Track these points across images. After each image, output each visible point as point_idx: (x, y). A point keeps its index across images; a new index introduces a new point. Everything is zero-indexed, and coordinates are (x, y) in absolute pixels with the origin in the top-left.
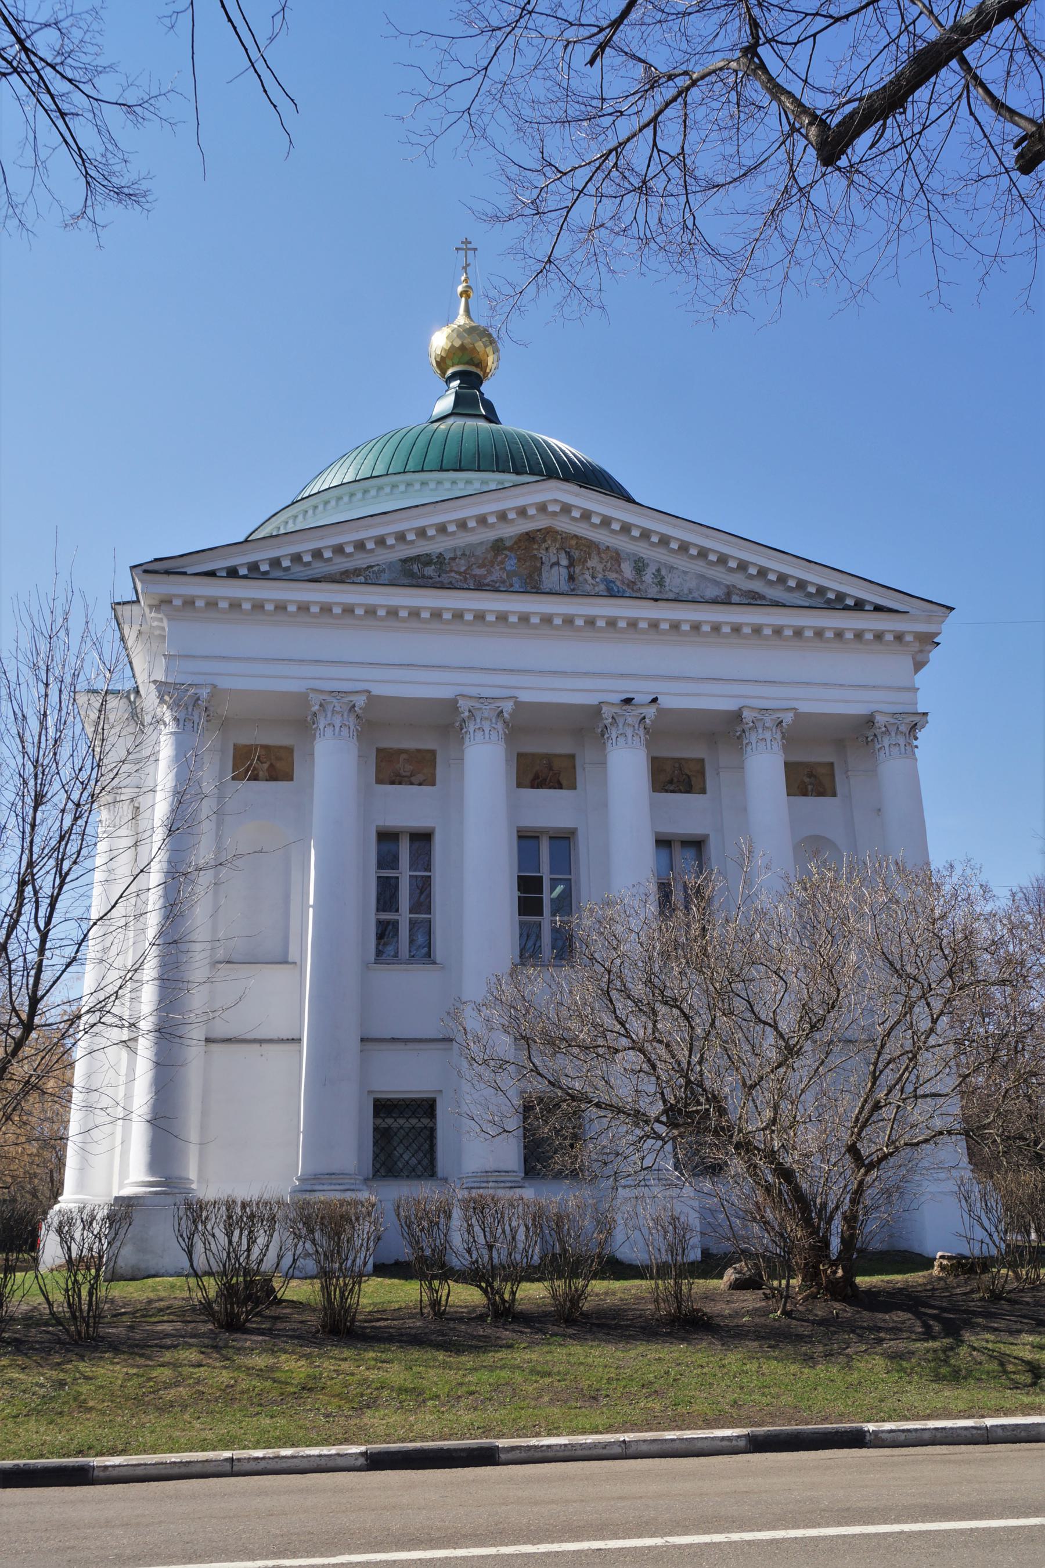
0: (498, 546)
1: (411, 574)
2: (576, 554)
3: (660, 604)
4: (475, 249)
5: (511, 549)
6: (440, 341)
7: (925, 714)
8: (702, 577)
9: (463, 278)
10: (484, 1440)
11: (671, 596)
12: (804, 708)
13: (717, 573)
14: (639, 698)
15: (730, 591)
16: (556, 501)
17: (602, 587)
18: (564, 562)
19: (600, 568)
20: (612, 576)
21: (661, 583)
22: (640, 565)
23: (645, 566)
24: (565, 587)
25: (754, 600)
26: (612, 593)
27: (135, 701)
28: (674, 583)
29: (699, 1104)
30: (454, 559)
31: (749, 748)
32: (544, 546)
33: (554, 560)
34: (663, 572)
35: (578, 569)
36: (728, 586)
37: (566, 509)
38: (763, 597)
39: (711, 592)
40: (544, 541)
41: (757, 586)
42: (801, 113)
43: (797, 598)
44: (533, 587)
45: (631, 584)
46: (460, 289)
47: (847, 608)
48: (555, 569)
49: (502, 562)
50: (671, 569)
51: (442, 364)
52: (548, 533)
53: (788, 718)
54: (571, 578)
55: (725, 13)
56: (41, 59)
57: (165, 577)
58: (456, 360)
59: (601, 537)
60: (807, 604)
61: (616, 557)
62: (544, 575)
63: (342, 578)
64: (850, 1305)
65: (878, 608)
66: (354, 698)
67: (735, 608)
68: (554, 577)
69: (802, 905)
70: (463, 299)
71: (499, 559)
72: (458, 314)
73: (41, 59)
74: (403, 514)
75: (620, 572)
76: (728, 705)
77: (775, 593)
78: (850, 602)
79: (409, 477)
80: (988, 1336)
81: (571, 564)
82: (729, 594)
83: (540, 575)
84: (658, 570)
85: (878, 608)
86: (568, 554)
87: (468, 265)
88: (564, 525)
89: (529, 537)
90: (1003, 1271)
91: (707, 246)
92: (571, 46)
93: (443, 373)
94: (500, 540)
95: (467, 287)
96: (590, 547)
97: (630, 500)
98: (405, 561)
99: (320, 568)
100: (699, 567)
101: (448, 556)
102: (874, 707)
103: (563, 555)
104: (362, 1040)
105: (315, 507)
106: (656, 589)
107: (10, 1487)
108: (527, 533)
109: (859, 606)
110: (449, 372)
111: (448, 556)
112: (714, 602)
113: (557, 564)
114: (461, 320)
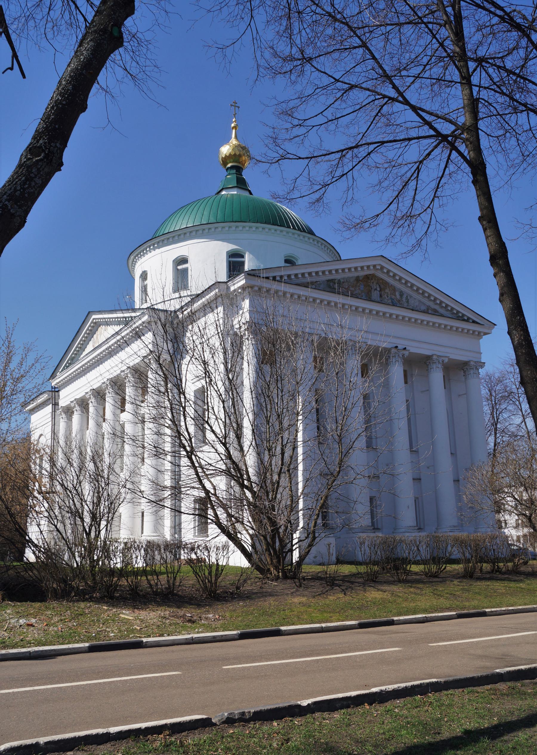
0: (357, 279)
1: (330, 287)
2: (382, 286)
3: (414, 312)
4: (239, 107)
5: (361, 281)
6: (225, 150)
8: (420, 301)
9: (234, 120)
11: (411, 308)
12: (452, 357)
13: (425, 301)
14: (400, 347)
15: (428, 307)
16: (380, 265)
17: (390, 301)
18: (378, 289)
19: (389, 293)
20: (393, 297)
21: (408, 302)
22: (402, 294)
23: (403, 294)
24: (379, 299)
25: (435, 313)
26: (394, 304)
28: (411, 302)
30: (343, 282)
31: (432, 370)
32: (372, 281)
33: (375, 288)
34: (409, 298)
35: (383, 292)
36: (428, 306)
37: (382, 268)
38: (438, 312)
39: (423, 308)
40: (372, 279)
41: (437, 307)
43: (448, 314)
44: (369, 299)
45: (399, 301)
46: (233, 125)
47: (464, 320)
48: (376, 291)
49: (359, 286)
50: (411, 297)
51: (225, 161)
52: (373, 276)
53: (446, 360)
54: (381, 296)
56: (431, 114)
57: (411, 311)
58: (232, 160)
60: (451, 316)
61: (394, 289)
62: (372, 293)
63: (306, 285)
65: (474, 322)
68: (375, 295)
70: (234, 130)
71: (358, 284)
72: (231, 138)
73: (431, 114)
75: (395, 295)
76: (465, 359)
77: (442, 311)
78: (466, 318)
79: (209, 226)
81: (380, 291)
82: (428, 309)
83: (371, 293)
84: (407, 297)
85: (474, 322)
86: (379, 286)
87: (236, 114)
94: (358, 277)
95: (237, 125)
96: (386, 284)
98: (328, 281)
99: (301, 280)
100: (420, 297)
101: (342, 281)
102: (471, 359)
103: (378, 286)
105: (204, 230)
106: (406, 304)
108: (366, 275)
109: (468, 320)
110: (229, 165)
111: (342, 281)
112: (424, 312)
113: (376, 289)
114: (234, 141)
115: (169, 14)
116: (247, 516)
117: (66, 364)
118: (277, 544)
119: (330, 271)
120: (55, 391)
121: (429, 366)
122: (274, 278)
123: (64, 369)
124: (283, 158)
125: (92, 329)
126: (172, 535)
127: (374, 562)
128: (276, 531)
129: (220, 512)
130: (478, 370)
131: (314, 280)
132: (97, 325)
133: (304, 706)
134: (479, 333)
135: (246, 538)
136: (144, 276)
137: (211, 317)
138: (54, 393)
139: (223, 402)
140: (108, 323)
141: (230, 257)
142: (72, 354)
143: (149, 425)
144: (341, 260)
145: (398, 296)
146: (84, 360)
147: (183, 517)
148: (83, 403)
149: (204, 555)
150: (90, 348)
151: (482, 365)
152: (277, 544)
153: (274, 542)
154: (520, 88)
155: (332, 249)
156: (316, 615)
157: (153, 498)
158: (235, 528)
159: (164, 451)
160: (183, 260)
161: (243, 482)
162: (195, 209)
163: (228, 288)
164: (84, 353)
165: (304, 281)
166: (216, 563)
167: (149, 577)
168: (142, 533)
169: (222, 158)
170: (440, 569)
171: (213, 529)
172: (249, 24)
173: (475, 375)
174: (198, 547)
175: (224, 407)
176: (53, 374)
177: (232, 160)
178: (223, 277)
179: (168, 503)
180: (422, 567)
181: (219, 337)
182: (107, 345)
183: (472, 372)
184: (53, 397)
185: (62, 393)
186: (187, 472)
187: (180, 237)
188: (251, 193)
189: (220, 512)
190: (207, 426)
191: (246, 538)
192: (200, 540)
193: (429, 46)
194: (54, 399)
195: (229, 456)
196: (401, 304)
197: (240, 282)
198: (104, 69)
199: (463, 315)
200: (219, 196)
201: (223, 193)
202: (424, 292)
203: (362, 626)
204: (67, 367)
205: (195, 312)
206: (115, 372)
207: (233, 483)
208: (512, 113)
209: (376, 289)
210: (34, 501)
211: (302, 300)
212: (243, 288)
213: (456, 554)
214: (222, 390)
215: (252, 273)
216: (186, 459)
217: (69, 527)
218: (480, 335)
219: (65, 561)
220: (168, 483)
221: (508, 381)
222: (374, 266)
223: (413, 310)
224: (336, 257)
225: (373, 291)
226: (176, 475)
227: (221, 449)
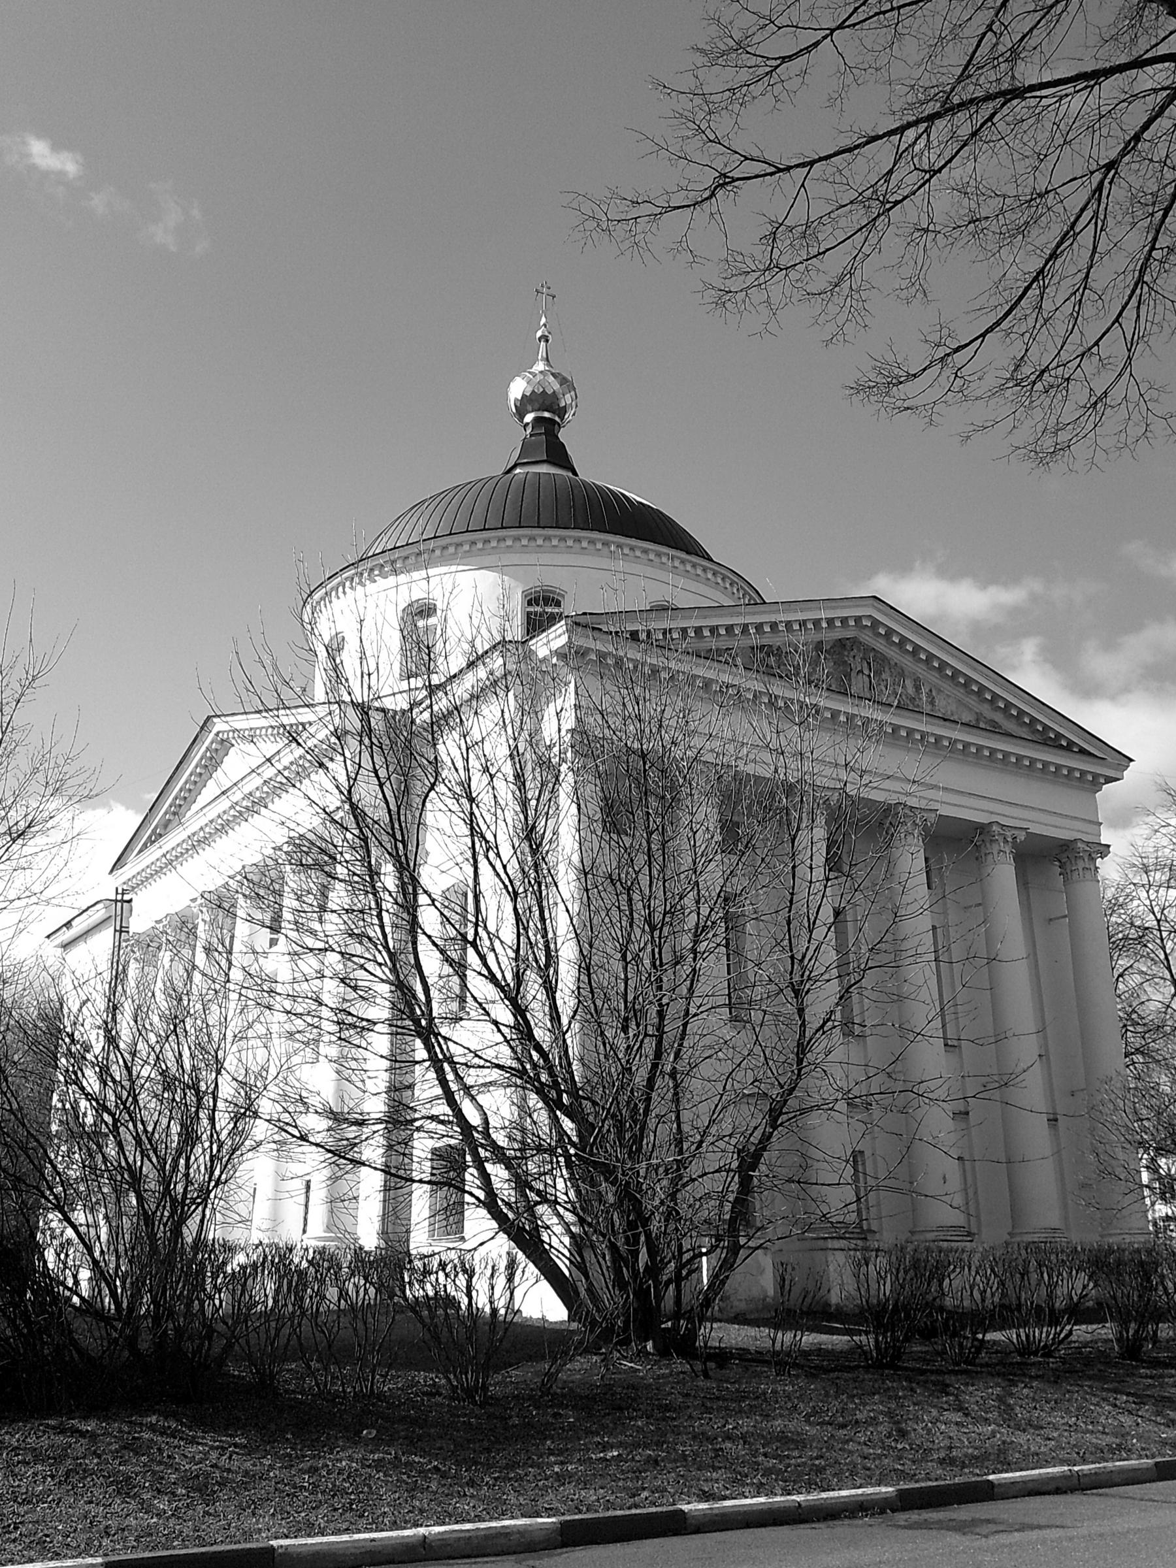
3: (947, 723)
6: (518, 388)
7: (1109, 846)
10: (870, 1490)
12: (1035, 829)
13: (986, 710)
15: (979, 716)
21: (932, 703)
25: (995, 729)
27: (705, 1363)
28: (940, 702)
29: (45, 1319)
32: (852, 654)
34: (934, 693)
37: (876, 623)
38: (1000, 727)
39: (967, 717)
41: (998, 717)
42: (748, 1224)
43: (1023, 732)
45: (913, 699)
46: (539, 334)
52: (854, 641)
53: (1022, 836)
55: (851, 1289)
57: (942, 722)
58: (537, 406)
59: (892, 654)
63: (707, 655)
64: (106, 1419)
66: (1016, 832)
67: (981, 732)
68: (858, 684)
69: (228, 981)
74: (1060, 718)
76: (893, 799)
77: (1010, 726)
79: (486, 534)
80: (645, 1142)
85: (1083, 751)
88: (867, 638)
89: (841, 644)
90: (236, 1373)
91: (471, 907)
92: (950, 1043)
93: (521, 418)
96: (883, 660)
97: (712, 560)
104: (967, 1113)
106: (930, 707)
107: (552, 1285)
113: (861, 671)
114: (540, 366)
115: (484, 734)
116: (561, 1186)
117: (150, 837)
118: (643, 1257)
119: (759, 627)
120: (123, 901)
121: (983, 850)
122: (634, 636)
123: (145, 846)
124: (725, 181)
125: (219, 747)
126: (384, 1233)
127: (900, 998)
128: (638, 1219)
129: (498, 1172)
130: (1094, 860)
131: (723, 645)
132: (224, 745)
133: (512, 380)
134: (1096, 776)
135: (558, 1241)
136: (334, 649)
137: (491, 711)
138: (119, 904)
139: (514, 896)
140: (251, 737)
141: (530, 603)
142: (166, 813)
143: (668, 1068)
144: (765, 603)
145: (911, 690)
146: (195, 821)
147: (379, 1161)
148: (185, 925)
149: (456, 1289)
150: (210, 790)
151: (1104, 850)
152: (643, 1257)
153: (635, 1254)
154: (274, 891)
155: (754, 595)
156: (859, 1482)
157: (330, 1142)
158: (534, 1217)
159: (347, 1139)
160: (426, 610)
161: (560, 1097)
162: (415, 519)
163: (529, 655)
164: (195, 807)
165: (703, 645)
166: (487, 1309)
167: (636, 745)
168: (304, 1231)
169: (516, 400)
170: (1057, 1334)
171: (478, 1222)
172: (803, 185)
173: (1088, 873)
174: (443, 1266)
175: (515, 909)
176: (119, 859)
177: (529, 408)
178: (516, 632)
179: (373, 1151)
180: (1107, 1331)
181: (188, 1167)
182: (907, 722)
183: (1081, 864)
184: (119, 912)
185: (140, 900)
186: (426, 1087)
187: (407, 562)
188: (575, 474)
189: (498, 1172)
190: (472, 957)
191: (558, 1241)
192: (444, 1249)
193: (786, 942)
194: (119, 918)
195: (524, 1030)
196: (918, 706)
197: (555, 639)
198: (489, 1216)
199: (1059, 736)
200: (510, 476)
201: (518, 471)
202: (969, 680)
203: (907, 1501)
204: (151, 841)
205: (1054, 1108)
206: (213, 882)
207: (533, 1100)
208: (929, 180)
209: (861, 671)
210: (153, 1206)
211: (825, 719)
212: (561, 654)
213: (250, 1154)
214: (513, 868)
215: (581, 620)
216: (483, 1212)
217: (212, 813)
218: (1096, 783)
219: (80, 1296)
220: (376, 1107)
221: (1136, 903)
222: (858, 619)
223: (945, 720)
224: (751, 598)
225: (853, 674)
226: (398, 1091)
227: (504, 1014)
